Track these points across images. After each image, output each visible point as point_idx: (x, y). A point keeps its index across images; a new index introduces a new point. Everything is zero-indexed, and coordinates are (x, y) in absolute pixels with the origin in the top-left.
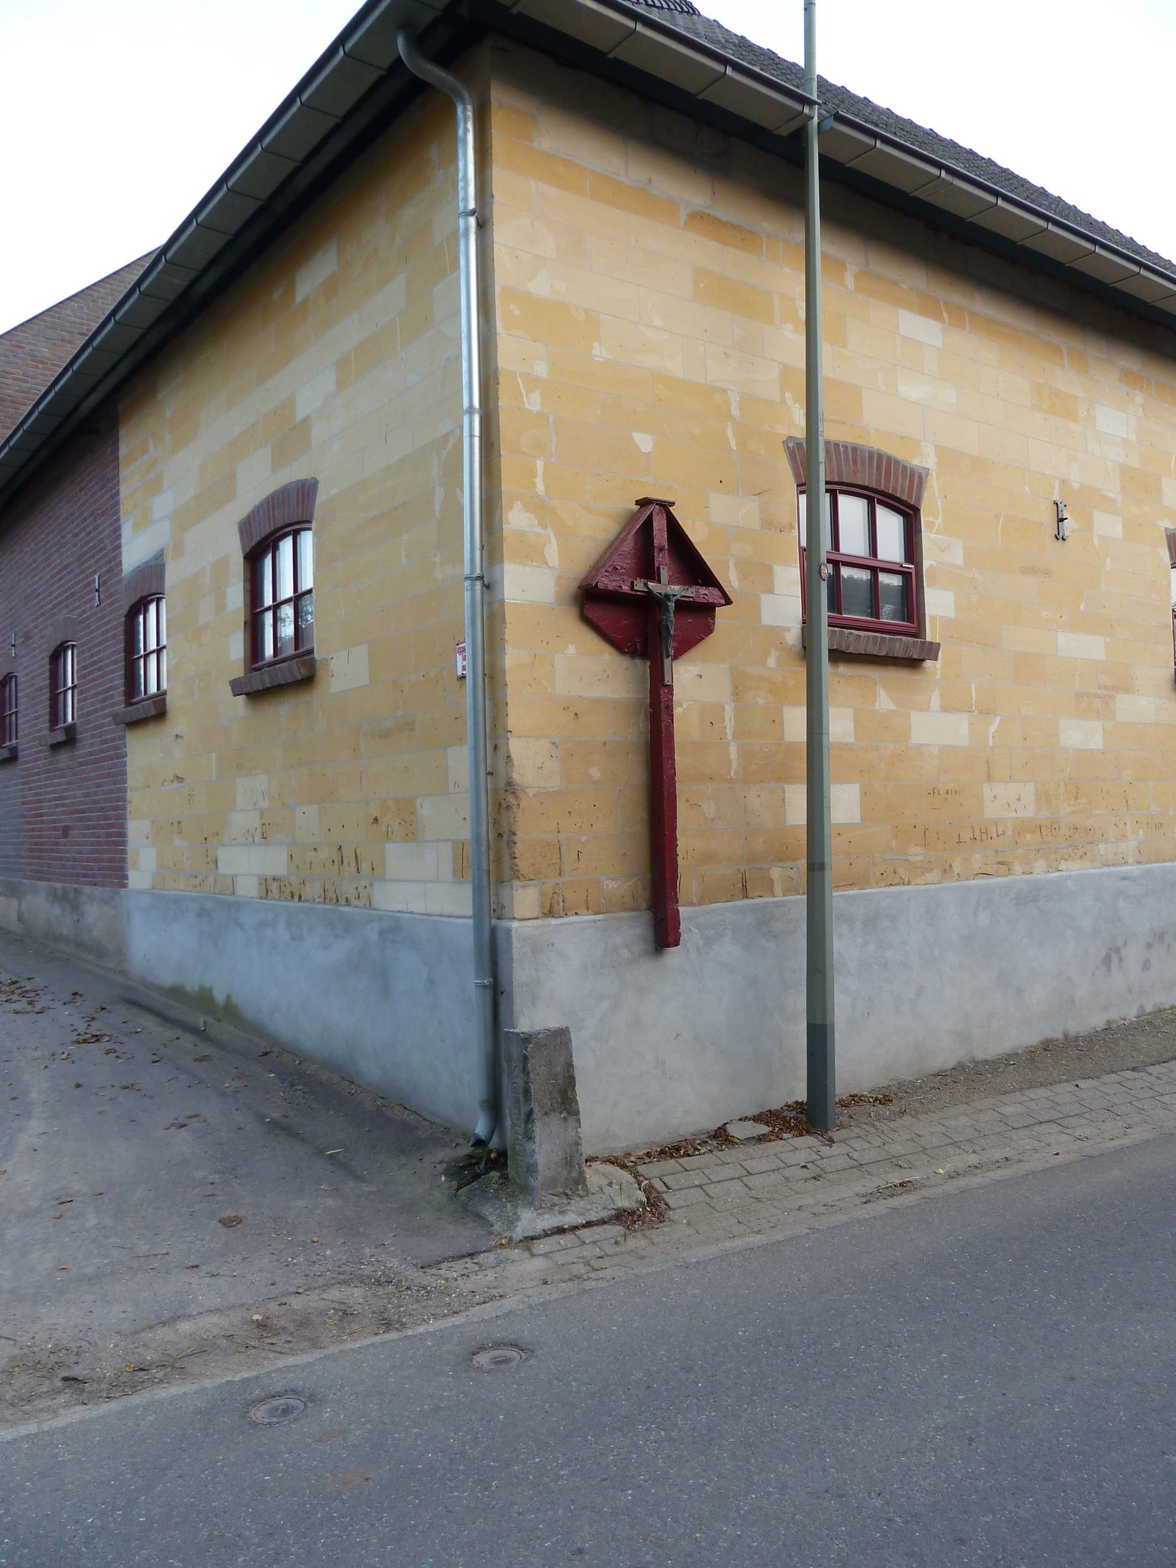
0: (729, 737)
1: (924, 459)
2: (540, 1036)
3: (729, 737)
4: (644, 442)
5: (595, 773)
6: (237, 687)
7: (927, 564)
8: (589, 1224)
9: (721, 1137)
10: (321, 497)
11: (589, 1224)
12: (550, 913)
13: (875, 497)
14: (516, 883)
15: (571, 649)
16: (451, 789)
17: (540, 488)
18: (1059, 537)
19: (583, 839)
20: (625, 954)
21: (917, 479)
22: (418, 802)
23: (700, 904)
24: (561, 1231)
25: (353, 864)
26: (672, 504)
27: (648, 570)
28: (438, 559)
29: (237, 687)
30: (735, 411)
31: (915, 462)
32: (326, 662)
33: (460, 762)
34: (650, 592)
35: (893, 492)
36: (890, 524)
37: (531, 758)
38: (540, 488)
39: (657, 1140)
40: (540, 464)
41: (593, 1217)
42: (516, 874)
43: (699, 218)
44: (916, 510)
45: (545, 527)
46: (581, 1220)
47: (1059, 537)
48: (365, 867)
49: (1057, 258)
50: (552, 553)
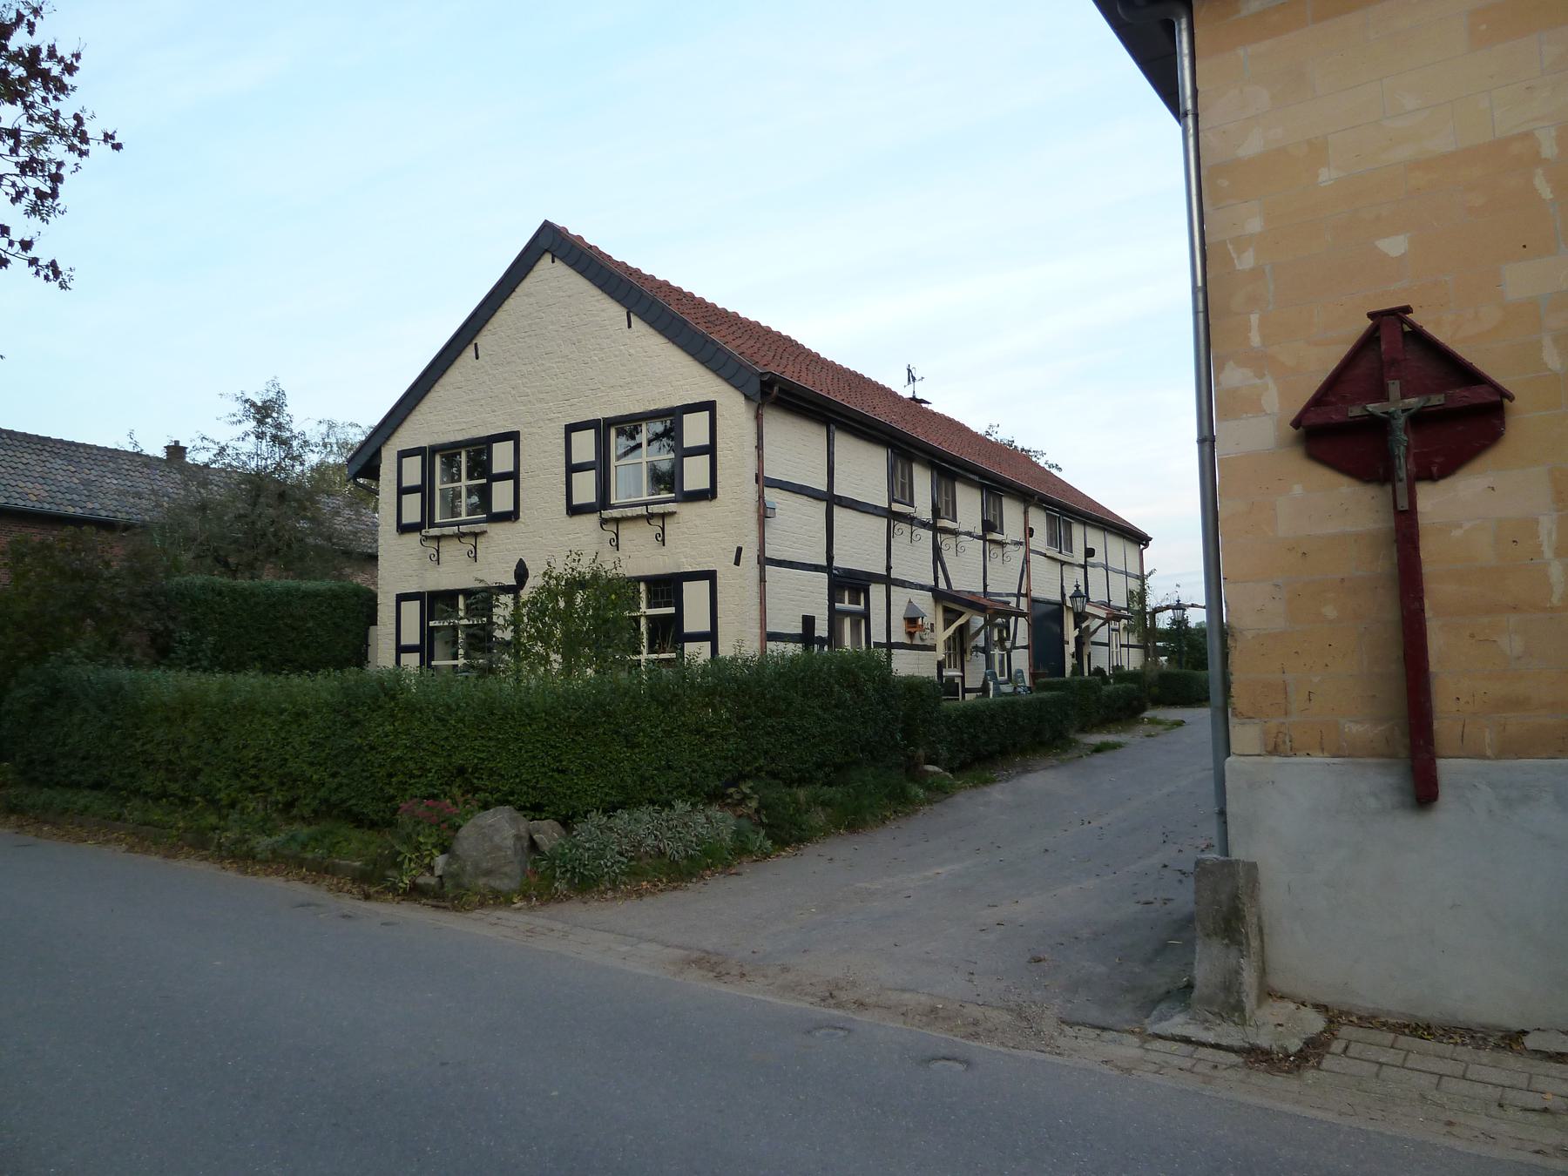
0: (1548, 553)
2: (819, 817)
3: (1548, 553)
5: (1330, 612)
8: (1217, 1046)
9: (1512, 1040)
11: (1217, 1046)
12: (1275, 751)
15: (1297, 489)
19: (1316, 680)
20: (1372, 803)
23: (1498, 757)
24: (1187, 1040)
26: (1408, 310)
30: (1549, 150)
34: (1371, 415)
39: (1420, 1014)
40: (1254, 319)
41: (1224, 1042)
45: (1261, 376)
49: (437, 387)
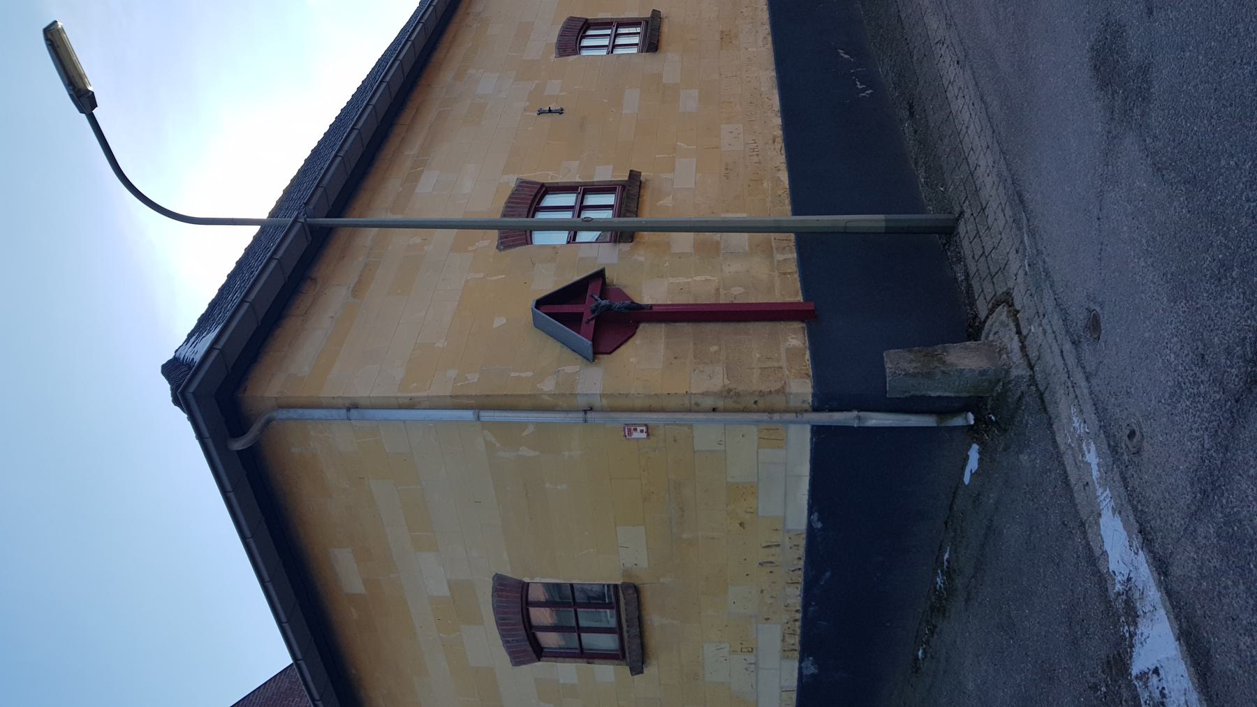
1: (511, 181)
4: (499, 321)
5: (714, 348)
6: (637, 669)
7: (578, 180)
10: (507, 572)
13: (535, 206)
14: (787, 390)
16: (722, 447)
17: (529, 374)
18: (561, 112)
21: (523, 184)
22: (729, 480)
25: (773, 550)
27: (579, 316)
28: (566, 454)
29: (637, 669)
30: (481, 275)
31: (513, 185)
32: (626, 572)
33: (707, 434)
35: (531, 197)
36: (550, 200)
37: (709, 380)
38: (529, 374)
42: (781, 391)
43: (357, 290)
44: (543, 185)
46: (1016, 338)
47: (561, 112)
48: (776, 538)
50: (569, 369)
